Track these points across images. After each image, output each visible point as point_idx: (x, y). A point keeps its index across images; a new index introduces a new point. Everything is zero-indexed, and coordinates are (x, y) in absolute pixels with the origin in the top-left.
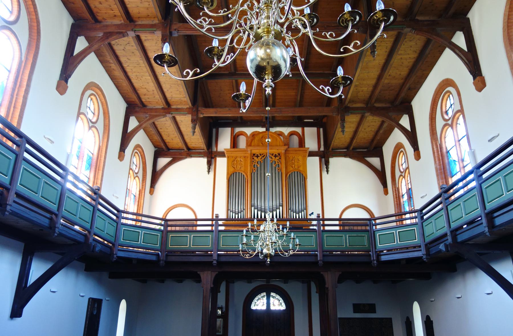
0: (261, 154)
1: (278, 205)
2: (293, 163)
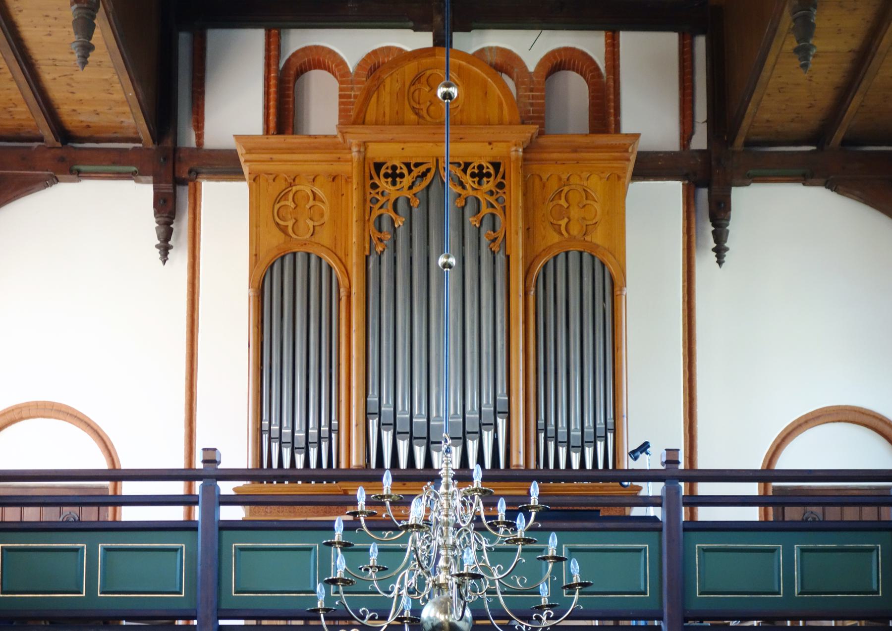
0: (413, 162)
1: (488, 409)
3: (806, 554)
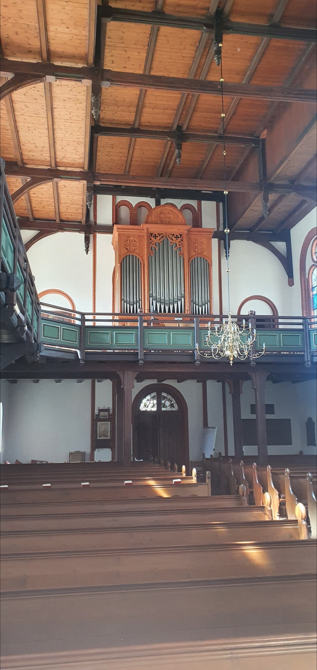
2: (197, 248)
3: (88, 355)
